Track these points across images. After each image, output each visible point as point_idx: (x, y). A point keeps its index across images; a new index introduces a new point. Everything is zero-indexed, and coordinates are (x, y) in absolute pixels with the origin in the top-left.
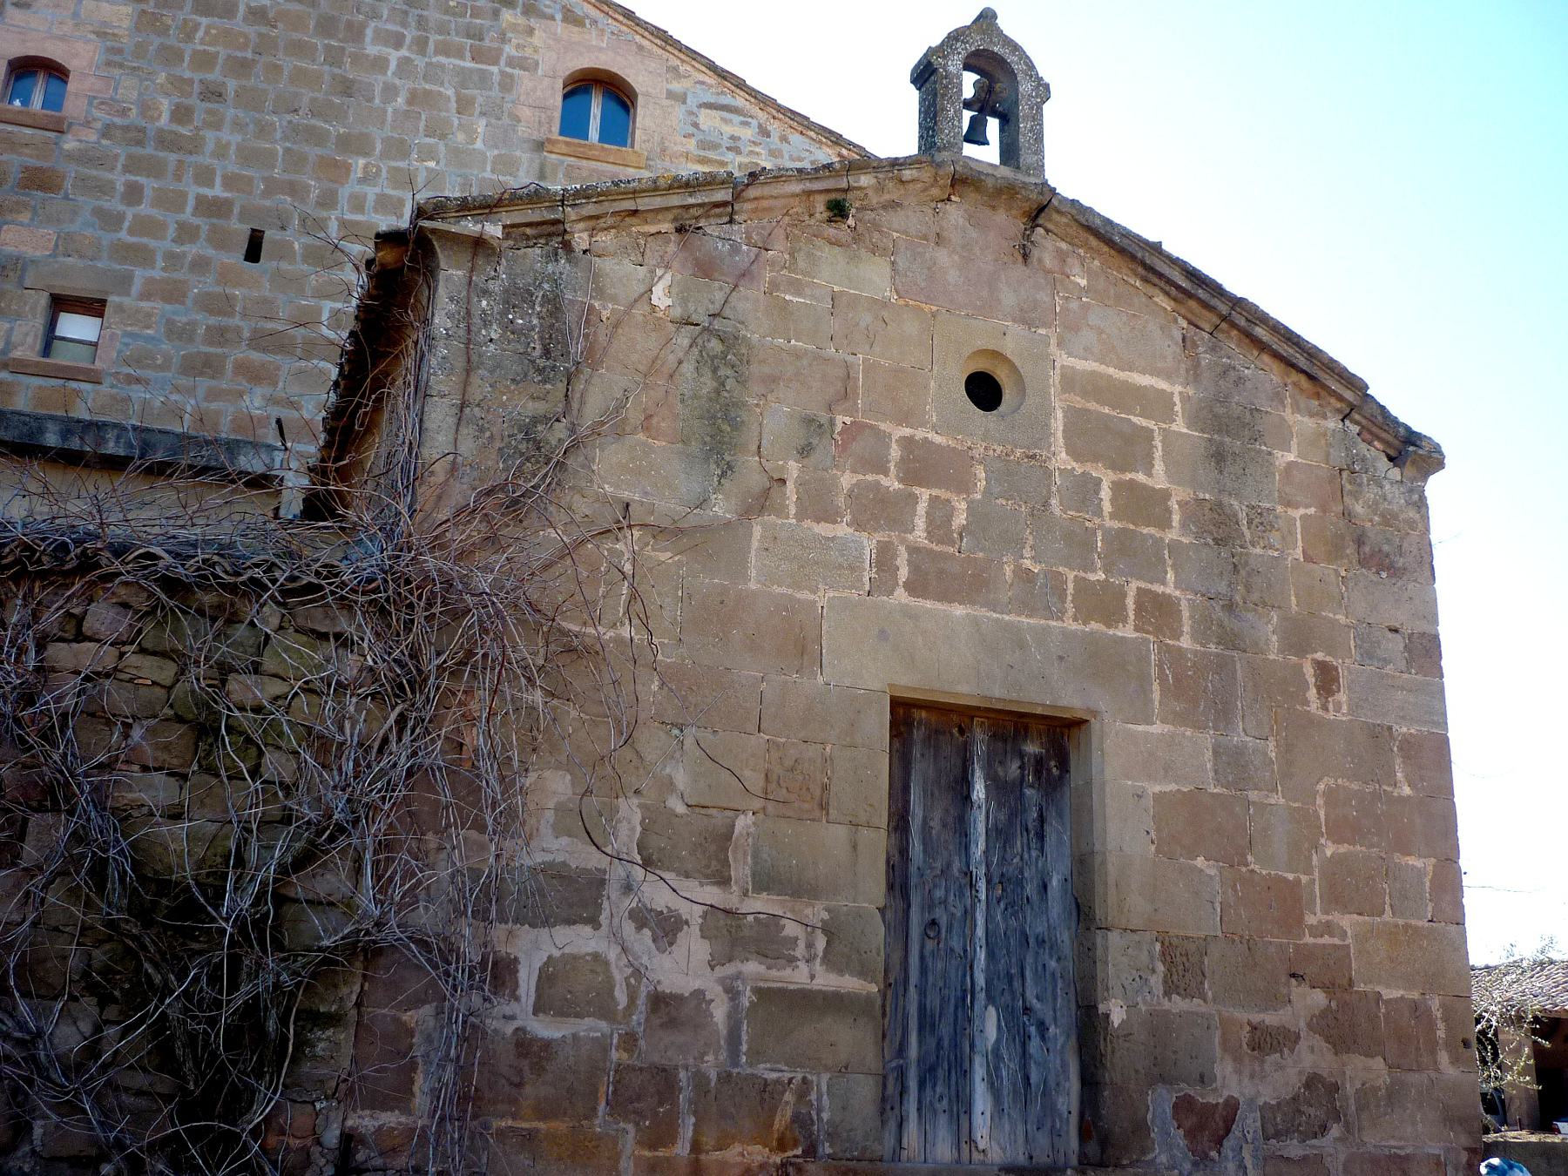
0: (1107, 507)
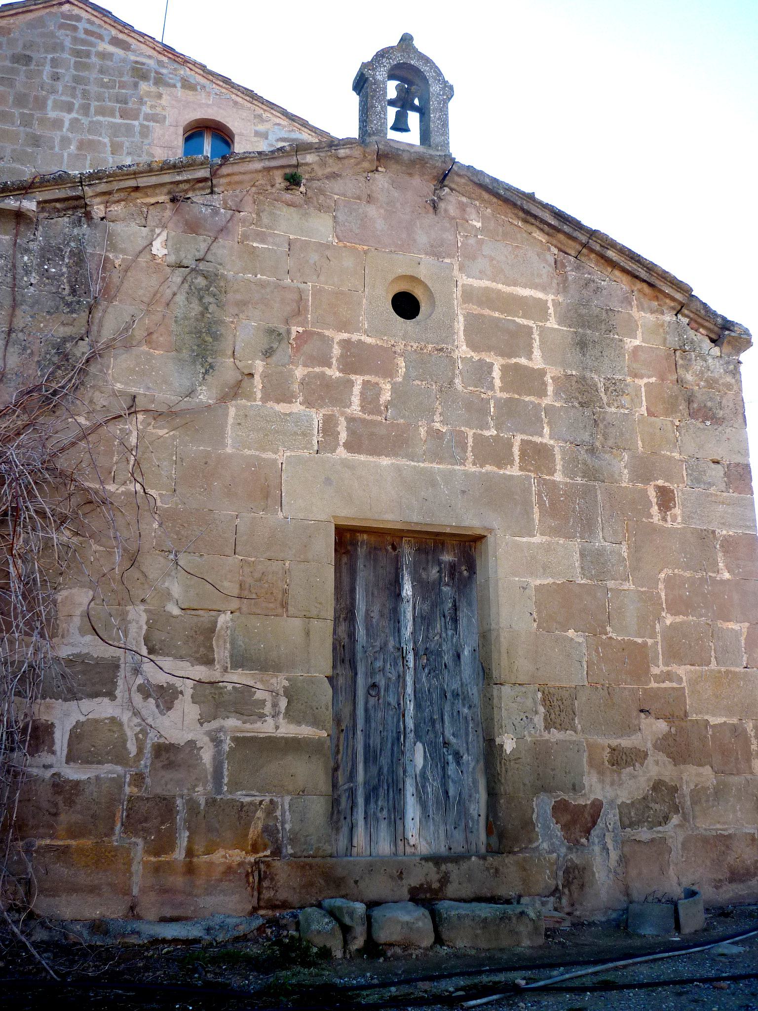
0: (498, 383)
